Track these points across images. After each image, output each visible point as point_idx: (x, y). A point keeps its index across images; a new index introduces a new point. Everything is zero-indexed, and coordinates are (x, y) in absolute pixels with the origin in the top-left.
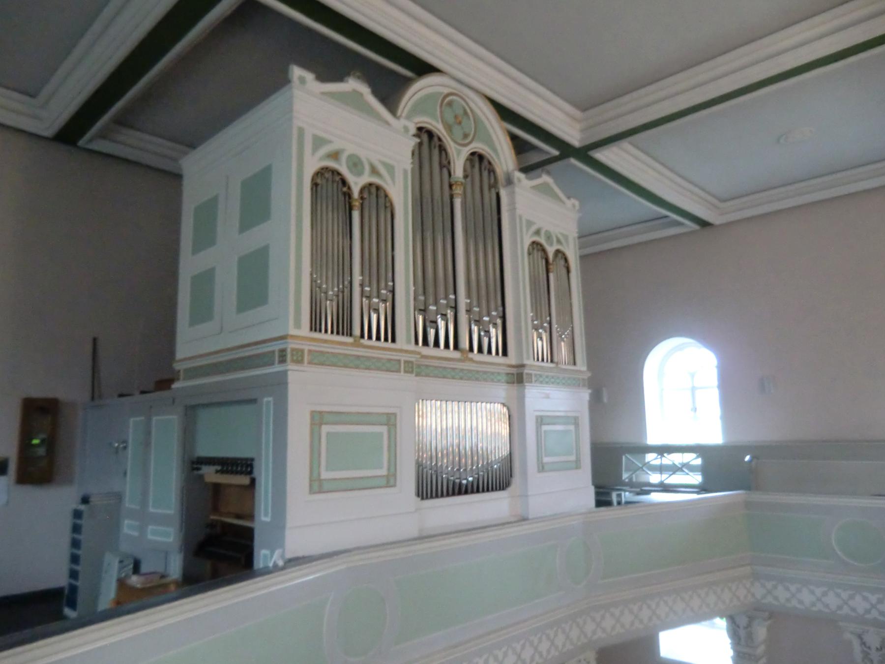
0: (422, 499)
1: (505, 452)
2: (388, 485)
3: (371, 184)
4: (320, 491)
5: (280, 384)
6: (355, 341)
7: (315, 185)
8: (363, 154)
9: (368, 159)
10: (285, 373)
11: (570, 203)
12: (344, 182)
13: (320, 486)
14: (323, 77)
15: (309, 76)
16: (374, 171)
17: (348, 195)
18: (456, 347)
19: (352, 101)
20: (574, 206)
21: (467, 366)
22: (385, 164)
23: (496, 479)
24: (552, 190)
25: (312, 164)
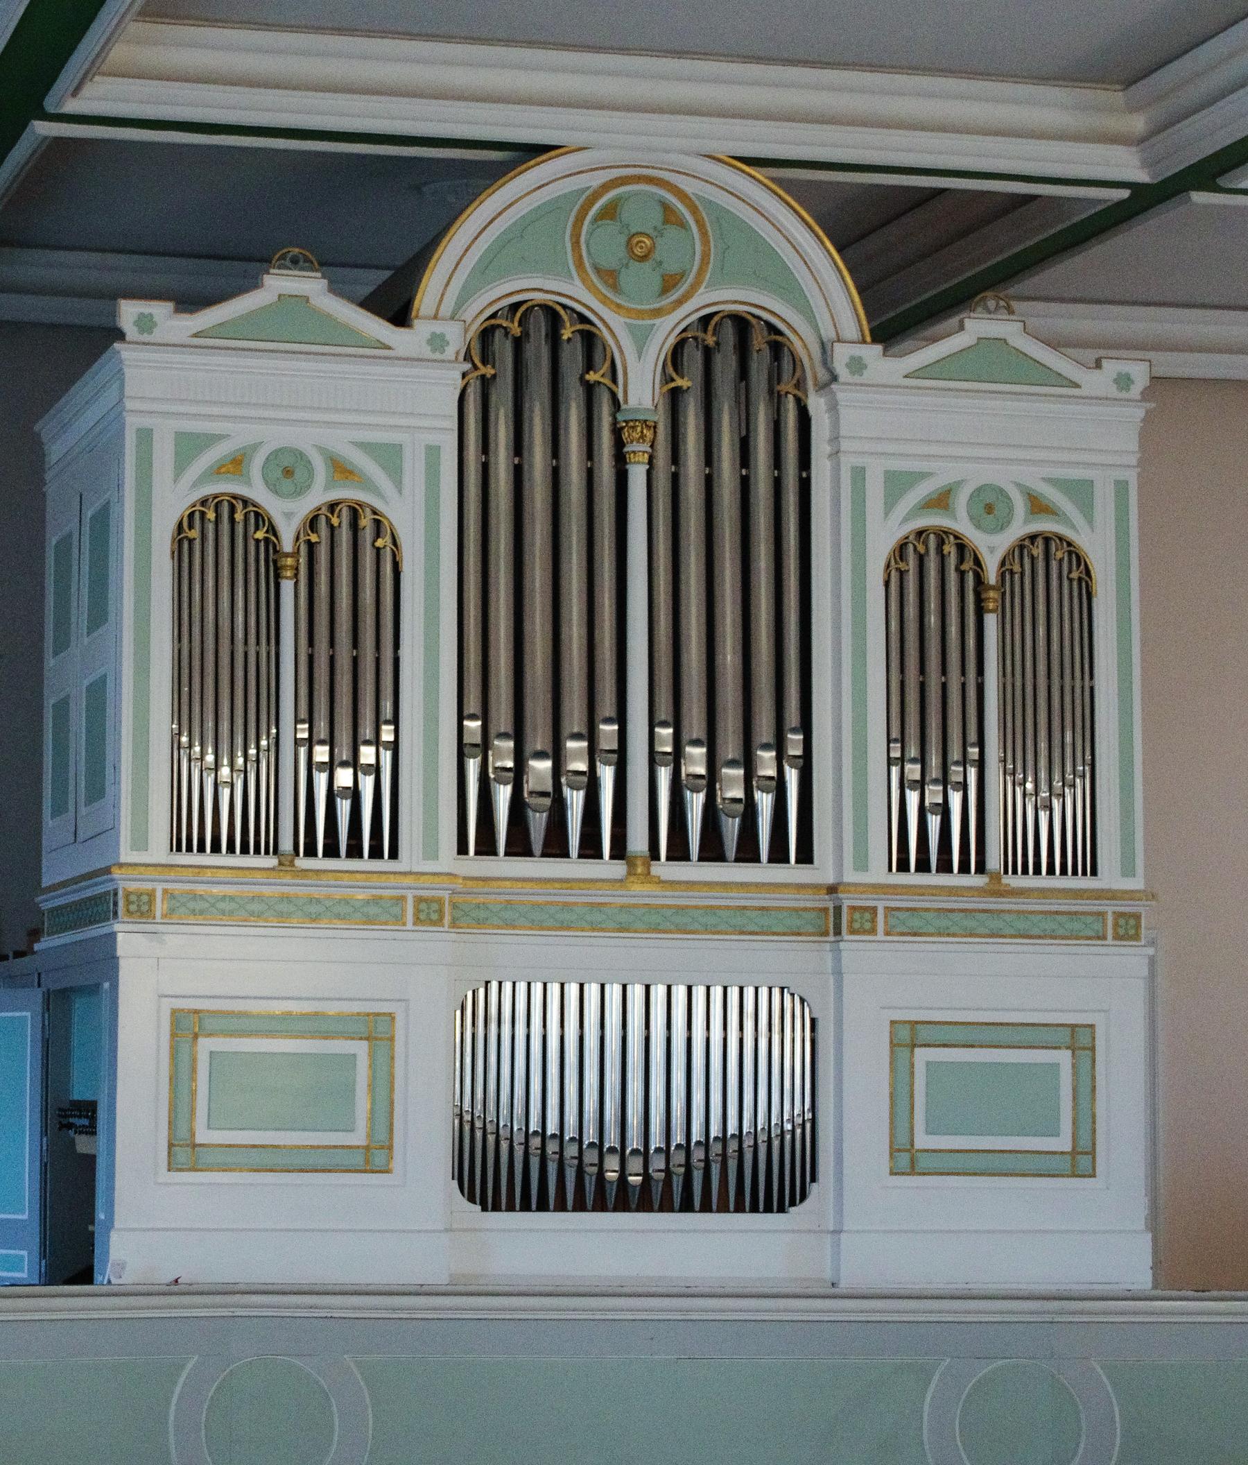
0: (484, 1209)
1: (798, 1107)
2: (368, 1169)
3: (1033, 538)
4: (913, 1171)
5: (105, 961)
6: (281, 864)
7: (181, 542)
8: (305, 439)
9: (321, 450)
10: (112, 936)
11: (1096, 382)
12: (261, 518)
13: (913, 1162)
14: (190, 301)
15: (160, 310)
16: (1038, 506)
17: (271, 544)
18: (619, 851)
19: (292, 329)
20: (1124, 381)
21: (639, 892)
22: (1065, 486)
23: (766, 1175)
24: (327, 319)
25: (172, 500)
